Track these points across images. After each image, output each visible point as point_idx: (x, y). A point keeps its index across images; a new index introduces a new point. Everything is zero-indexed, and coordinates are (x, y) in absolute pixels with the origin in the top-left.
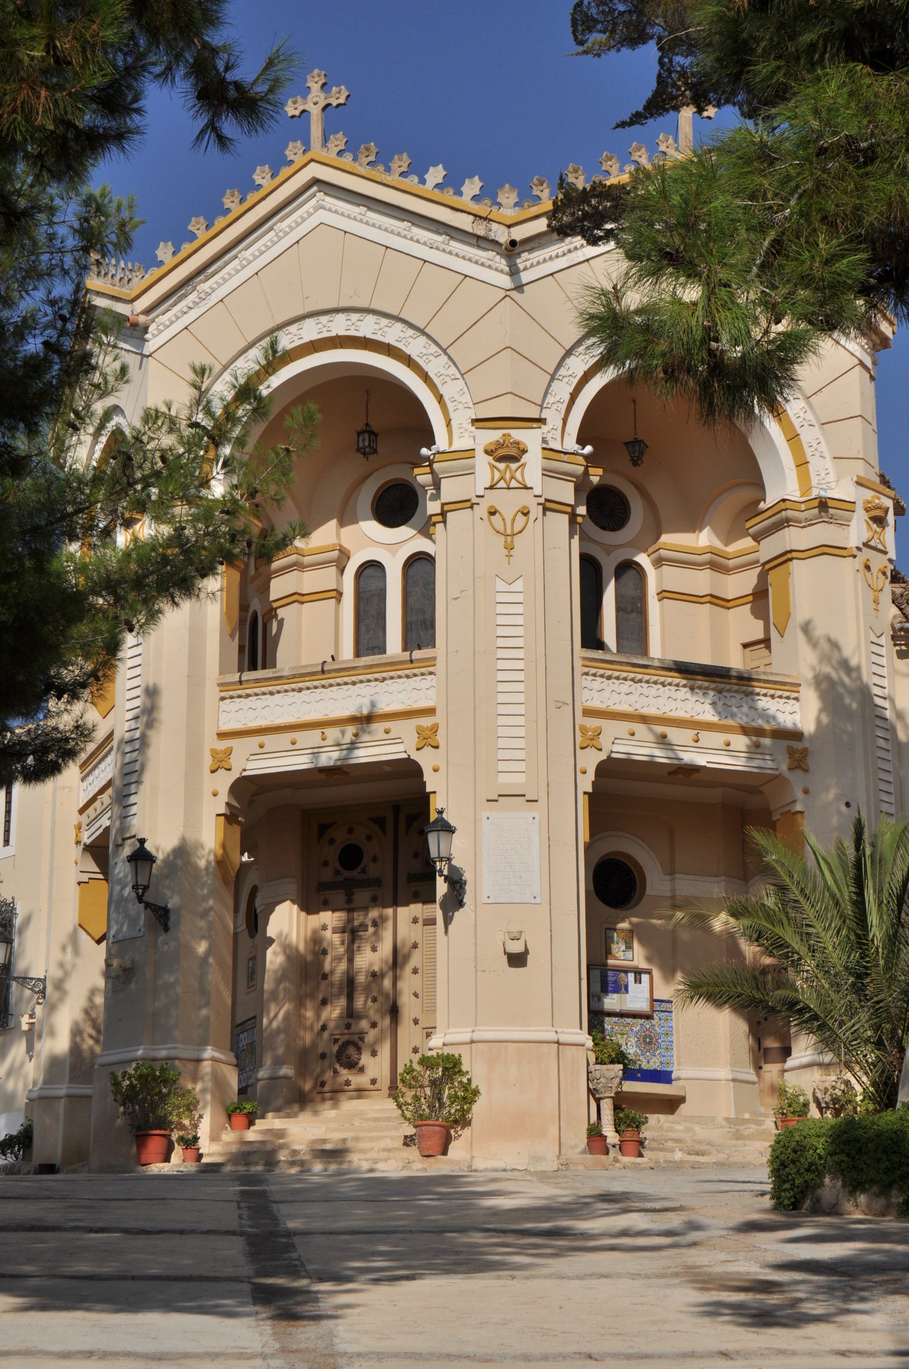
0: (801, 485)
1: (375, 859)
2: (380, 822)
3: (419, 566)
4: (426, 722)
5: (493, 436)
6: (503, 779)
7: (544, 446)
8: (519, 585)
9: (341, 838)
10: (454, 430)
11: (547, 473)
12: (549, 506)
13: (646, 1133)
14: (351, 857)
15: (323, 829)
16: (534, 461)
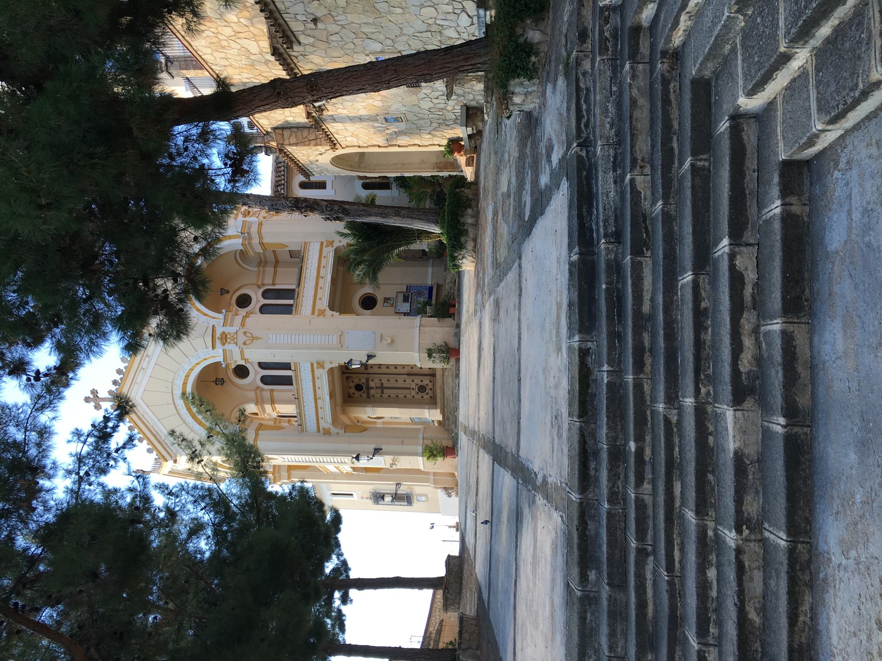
2: (348, 378)
3: (263, 366)
4: (315, 366)
5: (218, 342)
6: (335, 342)
8: (270, 336)
9: (353, 390)
10: (217, 355)
11: (231, 325)
12: (243, 324)
13: (214, 84)
14: (359, 388)
15: (349, 396)
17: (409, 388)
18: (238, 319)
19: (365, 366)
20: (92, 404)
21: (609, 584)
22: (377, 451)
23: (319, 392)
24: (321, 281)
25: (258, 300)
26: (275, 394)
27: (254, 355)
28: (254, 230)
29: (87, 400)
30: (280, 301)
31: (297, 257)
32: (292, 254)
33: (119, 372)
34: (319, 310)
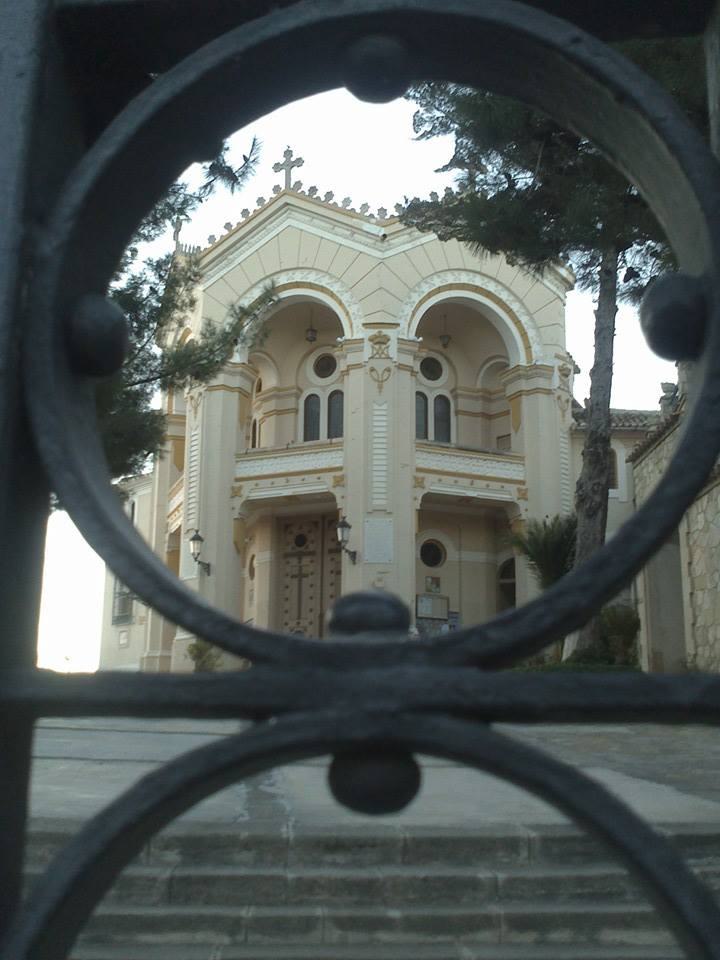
0: (527, 358)
1: (312, 542)
3: (336, 397)
4: (339, 473)
5: (374, 332)
7: (523, 487)
8: (384, 407)
9: (296, 531)
10: (354, 329)
11: (400, 350)
12: (400, 367)
15: (287, 527)
16: (393, 346)
17: (299, 617)
18: (409, 360)
19: (338, 548)
20: (282, 160)
21: (172, 879)
22: (206, 568)
23: (297, 479)
24: (466, 482)
25: (435, 389)
26: (291, 416)
27: (355, 388)
28: (541, 383)
29: (288, 153)
30: (436, 423)
31: (500, 446)
32: (504, 439)
33: (313, 190)
34: (423, 479)
